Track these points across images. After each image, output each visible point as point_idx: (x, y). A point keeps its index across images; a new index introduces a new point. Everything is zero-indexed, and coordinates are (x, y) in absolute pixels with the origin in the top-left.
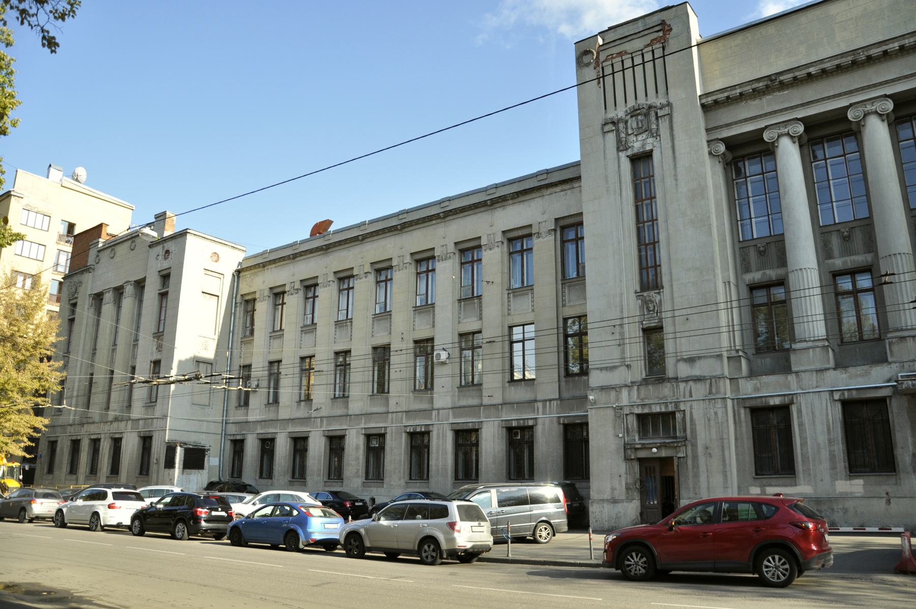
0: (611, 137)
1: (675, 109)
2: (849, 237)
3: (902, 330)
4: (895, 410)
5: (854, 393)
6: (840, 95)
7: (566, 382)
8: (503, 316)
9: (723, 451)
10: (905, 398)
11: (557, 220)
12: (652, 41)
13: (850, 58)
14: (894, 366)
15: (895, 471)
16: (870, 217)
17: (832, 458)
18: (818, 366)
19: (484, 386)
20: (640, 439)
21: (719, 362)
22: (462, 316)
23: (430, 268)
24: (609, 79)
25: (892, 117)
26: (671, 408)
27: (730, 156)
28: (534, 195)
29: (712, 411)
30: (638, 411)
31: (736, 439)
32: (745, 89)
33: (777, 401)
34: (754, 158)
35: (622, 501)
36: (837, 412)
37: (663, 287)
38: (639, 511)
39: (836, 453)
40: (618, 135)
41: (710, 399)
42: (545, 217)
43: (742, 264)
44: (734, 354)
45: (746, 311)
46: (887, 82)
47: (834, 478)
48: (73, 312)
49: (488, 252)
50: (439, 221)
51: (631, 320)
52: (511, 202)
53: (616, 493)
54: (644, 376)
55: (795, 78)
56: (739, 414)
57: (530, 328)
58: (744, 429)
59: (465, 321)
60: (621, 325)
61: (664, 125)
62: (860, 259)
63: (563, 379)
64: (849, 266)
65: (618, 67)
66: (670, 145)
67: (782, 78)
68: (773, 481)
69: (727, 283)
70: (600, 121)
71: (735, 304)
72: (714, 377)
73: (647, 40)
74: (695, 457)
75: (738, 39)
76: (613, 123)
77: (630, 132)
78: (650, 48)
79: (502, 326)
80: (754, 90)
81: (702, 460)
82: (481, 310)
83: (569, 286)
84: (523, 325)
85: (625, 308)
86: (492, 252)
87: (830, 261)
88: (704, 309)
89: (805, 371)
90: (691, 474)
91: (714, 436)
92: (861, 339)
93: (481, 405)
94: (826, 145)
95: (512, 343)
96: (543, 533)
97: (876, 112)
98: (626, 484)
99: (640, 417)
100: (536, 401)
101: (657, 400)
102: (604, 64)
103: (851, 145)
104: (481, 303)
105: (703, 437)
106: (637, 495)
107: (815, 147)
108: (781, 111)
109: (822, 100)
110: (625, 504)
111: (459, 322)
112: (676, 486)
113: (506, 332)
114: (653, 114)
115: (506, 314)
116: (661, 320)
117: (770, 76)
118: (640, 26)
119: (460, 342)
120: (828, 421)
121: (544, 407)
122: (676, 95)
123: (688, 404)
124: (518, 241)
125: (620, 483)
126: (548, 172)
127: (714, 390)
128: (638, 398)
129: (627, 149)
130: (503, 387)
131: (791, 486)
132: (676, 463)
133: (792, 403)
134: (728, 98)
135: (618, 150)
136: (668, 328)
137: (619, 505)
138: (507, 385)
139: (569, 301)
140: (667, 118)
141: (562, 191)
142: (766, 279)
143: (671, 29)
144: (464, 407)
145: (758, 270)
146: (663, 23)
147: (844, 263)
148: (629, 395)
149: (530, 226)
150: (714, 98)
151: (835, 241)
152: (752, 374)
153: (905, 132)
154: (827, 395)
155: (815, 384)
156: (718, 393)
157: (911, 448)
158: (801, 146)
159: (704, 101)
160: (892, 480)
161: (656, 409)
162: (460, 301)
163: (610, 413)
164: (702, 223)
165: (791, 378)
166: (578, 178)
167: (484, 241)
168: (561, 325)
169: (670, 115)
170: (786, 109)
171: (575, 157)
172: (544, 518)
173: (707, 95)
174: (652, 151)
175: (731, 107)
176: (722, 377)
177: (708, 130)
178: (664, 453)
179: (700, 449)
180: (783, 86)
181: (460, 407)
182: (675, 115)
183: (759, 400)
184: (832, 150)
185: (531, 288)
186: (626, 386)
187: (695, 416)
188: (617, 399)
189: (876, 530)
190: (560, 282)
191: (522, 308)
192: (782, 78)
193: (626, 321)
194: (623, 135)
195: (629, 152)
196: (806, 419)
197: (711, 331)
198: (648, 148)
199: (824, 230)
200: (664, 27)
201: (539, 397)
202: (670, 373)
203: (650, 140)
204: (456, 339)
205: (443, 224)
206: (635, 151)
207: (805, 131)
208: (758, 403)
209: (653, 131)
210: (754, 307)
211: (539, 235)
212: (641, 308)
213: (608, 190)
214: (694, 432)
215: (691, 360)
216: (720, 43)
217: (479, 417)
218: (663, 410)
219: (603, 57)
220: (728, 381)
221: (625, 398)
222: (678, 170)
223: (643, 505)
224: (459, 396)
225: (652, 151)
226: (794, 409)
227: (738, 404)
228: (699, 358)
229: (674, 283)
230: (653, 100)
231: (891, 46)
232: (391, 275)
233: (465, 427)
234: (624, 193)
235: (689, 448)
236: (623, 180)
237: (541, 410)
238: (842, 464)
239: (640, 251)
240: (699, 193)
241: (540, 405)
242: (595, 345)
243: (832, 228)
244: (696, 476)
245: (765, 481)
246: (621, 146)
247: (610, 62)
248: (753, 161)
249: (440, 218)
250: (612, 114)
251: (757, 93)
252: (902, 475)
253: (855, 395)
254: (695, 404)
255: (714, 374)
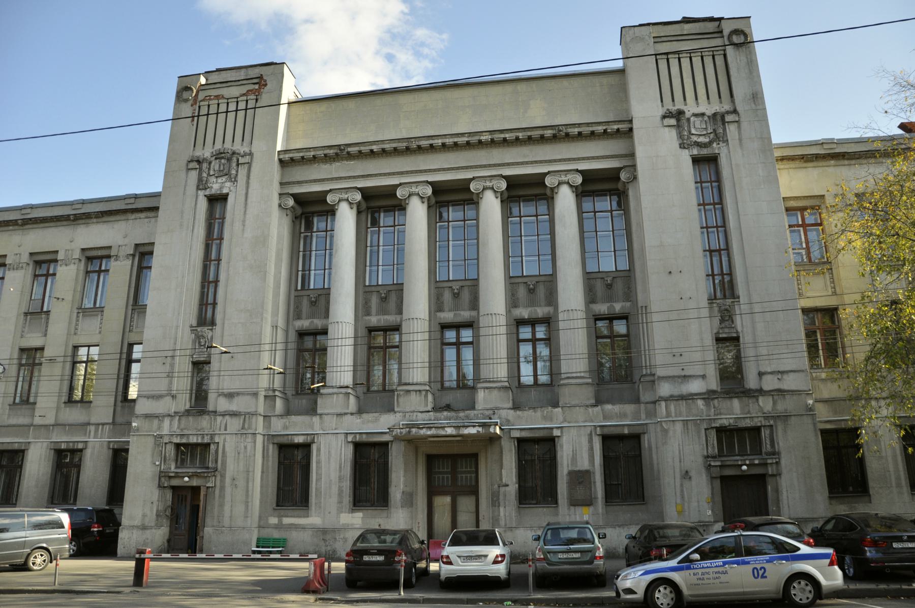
0: (194, 175)
1: (254, 160)
2: (386, 298)
3: (409, 384)
4: (394, 454)
5: (364, 436)
6: (394, 174)
7: (122, 407)
8: (68, 334)
9: (248, 482)
10: (403, 443)
11: (137, 245)
12: (248, 91)
13: (405, 144)
14: (398, 415)
15: (387, 506)
16: (477, 280)
17: (340, 494)
18: (339, 411)
19: (38, 405)
20: (176, 467)
21: (254, 400)
22: (26, 330)
23: (103, 268)
24: (203, 119)
25: (506, 195)
26: (206, 440)
27: (299, 211)
28: (118, 217)
29: (242, 445)
30: (177, 440)
31: (263, 472)
32: (318, 153)
33: (299, 440)
34: (529, 201)
35: (151, 528)
36: (348, 452)
37: (739, 297)
38: (167, 537)
39: (344, 489)
40: (200, 174)
41: (242, 433)
42: (126, 241)
43: (294, 311)
44: (271, 393)
45: (292, 354)
46: (430, 171)
47: (340, 511)
48: (727, 316)
49: (64, 267)
50: (16, 227)
51: (183, 353)
52: (95, 220)
53: (147, 520)
54: (188, 407)
55: (505, 140)
56: (268, 450)
57: (94, 351)
58: (270, 463)
59: (29, 335)
60: (173, 357)
61: (243, 172)
62: (541, 311)
63: (119, 404)
64: (382, 324)
65: (213, 109)
66: (244, 192)
67: (349, 149)
68: (290, 513)
69: (275, 327)
70: (187, 158)
71: (279, 346)
72: (249, 413)
73: (244, 89)
74: (222, 488)
75: (324, 106)
76: (198, 162)
77: (212, 173)
78: (245, 98)
79: (66, 346)
80: (326, 155)
81: (228, 490)
82: (47, 326)
83: (139, 313)
84: (89, 346)
85: (179, 340)
86: (68, 267)
87: (367, 318)
88: (248, 349)
89: (328, 414)
90: (217, 504)
91: (241, 468)
92: (384, 390)
93: (32, 425)
94: (451, 208)
95: (74, 363)
96: (38, 559)
97: (568, 183)
98: (157, 511)
99: (178, 446)
100: (89, 424)
101: (195, 431)
102: (202, 103)
103: (543, 208)
104: (48, 319)
105: (232, 467)
106: (166, 523)
107: (512, 204)
108: (345, 178)
109: (524, 162)
110: (154, 530)
111: (22, 336)
112: (200, 514)
113: (70, 352)
114: (235, 159)
115: (73, 332)
116: (209, 356)
117: (339, 145)
118: (242, 75)
119: (20, 359)
120: (341, 459)
121: (96, 431)
122: (258, 147)
123: (222, 437)
124: (95, 260)
125: (151, 510)
126: (136, 197)
127: (246, 426)
128: (178, 428)
129: (206, 189)
130: (58, 409)
131: (304, 517)
132: (202, 493)
133: (313, 442)
134: (303, 158)
135: (198, 188)
136: (215, 365)
137: (148, 532)
138: (63, 405)
139: (137, 327)
140: (246, 166)
141: (147, 218)
142: (312, 327)
143: (266, 85)
144: (14, 426)
145: (450, 311)
146: (261, 77)
147: (379, 321)
148: (171, 424)
149: (110, 247)
150: (291, 155)
151: (374, 301)
152: (288, 412)
153: (587, 205)
154: (343, 436)
155: (334, 426)
156: (249, 428)
157: (402, 487)
158: (429, 207)
159: (281, 157)
160: (385, 514)
161: (193, 440)
162: (26, 314)
163: (151, 440)
164: (260, 270)
165: (316, 419)
166: (156, 209)
167: (60, 256)
168: (125, 350)
169: (249, 164)
170: (350, 177)
171: (157, 187)
172: (44, 545)
173: (285, 152)
174: (227, 194)
175: (305, 167)
176: (255, 414)
177: (282, 184)
178: (195, 483)
179: (228, 480)
180: (350, 156)
181: (8, 426)
182: (254, 165)
183: (286, 438)
184: (527, 209)
185: (101, 309)
186: (169, 415)
187: (227, 449)
188: (159, 428)
189: (297, 556)
190: (130, 308)
191: (89, 328)
192: (349, 149)
193: (178, 353)
194: (205, 175)
195: (208, 192)
196: (323, 457)
197: (251, 372)
198: (225, 191)
199: (513, 280)
200: (261, 82)
201: (93, 420)
202: (211, 407)
203: (228, 184)
204: (16, 355)
205: (20, 232)
206: (213, 192)
207: (433, 192)
208: (284, 440)
209: (233, 176)
210: (300, 351)
211: (117, 257)
212: (194, 342)
213: (181, 225)
214: (224, 463)
215: (230, 396)
216: (309, 106)
217: (28, 438)
218: (200, 441)
219: (201, 97)
220: (261, 419)
221: (166, 427)
222: (247, 216)
223: (171, 532)
224: (9, 415)
225: (227, 194)
226: (314, 447)
227: (268, 440)
228: (238, 394)
229: (226, 322)
230: (238, 147)
231: (436, 141)
232: (55, 269)
233: (10, 447)
234: (196, 230)
235: (218, 478)
236: (197, 217)
237: (92, 433)
238: (347, 499)
239: (203, 287)
240: (261, 240)
241: (93, 428)
242: (46, 378)
243: (373, 289)
244: (222, 505)
245: (282, 512)
246: (201, 185)
247: (207, 103)
248: (387, 214)
249: (70, 220)
250: (199, 153)
251: (327, 159)
252: (393, 510)
253: (365, 438)
254: (228, 437)
255: (249, 411)
